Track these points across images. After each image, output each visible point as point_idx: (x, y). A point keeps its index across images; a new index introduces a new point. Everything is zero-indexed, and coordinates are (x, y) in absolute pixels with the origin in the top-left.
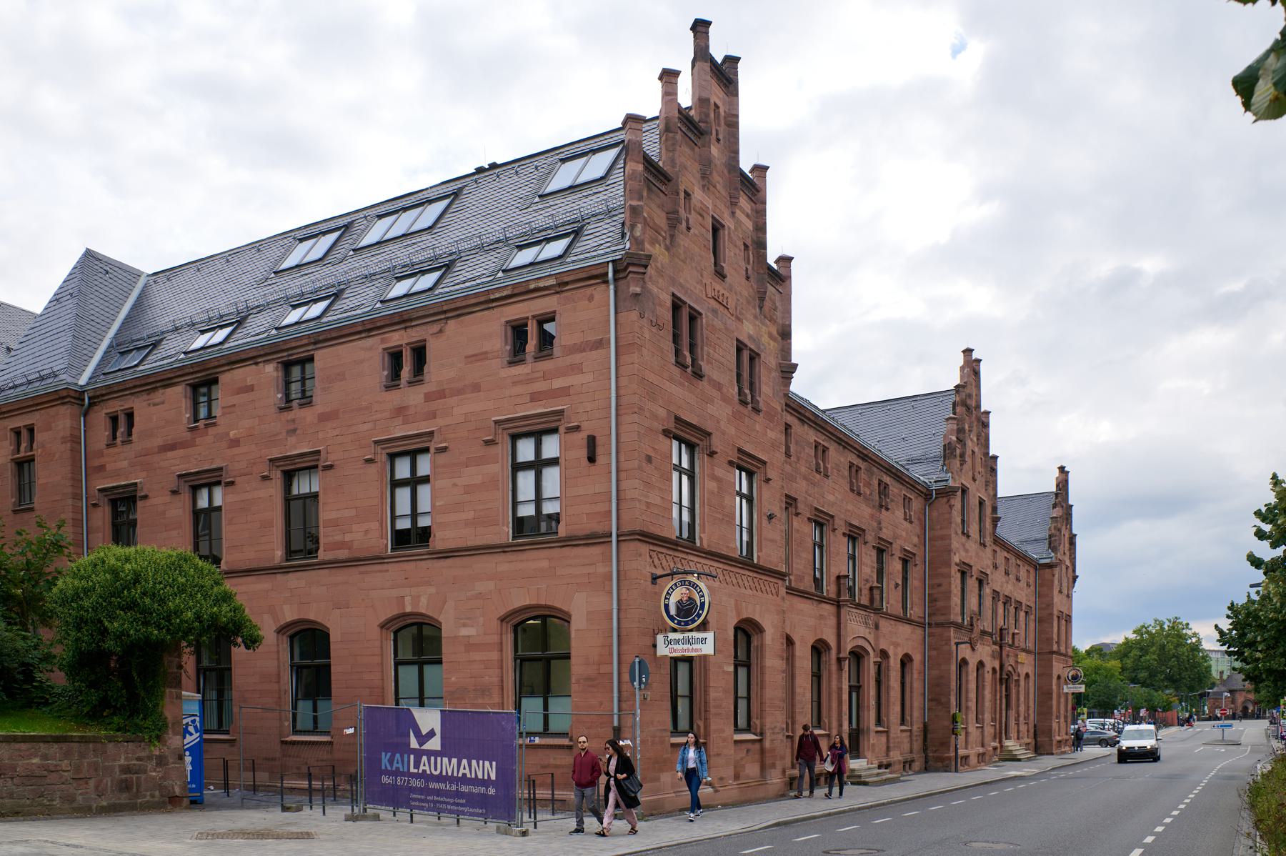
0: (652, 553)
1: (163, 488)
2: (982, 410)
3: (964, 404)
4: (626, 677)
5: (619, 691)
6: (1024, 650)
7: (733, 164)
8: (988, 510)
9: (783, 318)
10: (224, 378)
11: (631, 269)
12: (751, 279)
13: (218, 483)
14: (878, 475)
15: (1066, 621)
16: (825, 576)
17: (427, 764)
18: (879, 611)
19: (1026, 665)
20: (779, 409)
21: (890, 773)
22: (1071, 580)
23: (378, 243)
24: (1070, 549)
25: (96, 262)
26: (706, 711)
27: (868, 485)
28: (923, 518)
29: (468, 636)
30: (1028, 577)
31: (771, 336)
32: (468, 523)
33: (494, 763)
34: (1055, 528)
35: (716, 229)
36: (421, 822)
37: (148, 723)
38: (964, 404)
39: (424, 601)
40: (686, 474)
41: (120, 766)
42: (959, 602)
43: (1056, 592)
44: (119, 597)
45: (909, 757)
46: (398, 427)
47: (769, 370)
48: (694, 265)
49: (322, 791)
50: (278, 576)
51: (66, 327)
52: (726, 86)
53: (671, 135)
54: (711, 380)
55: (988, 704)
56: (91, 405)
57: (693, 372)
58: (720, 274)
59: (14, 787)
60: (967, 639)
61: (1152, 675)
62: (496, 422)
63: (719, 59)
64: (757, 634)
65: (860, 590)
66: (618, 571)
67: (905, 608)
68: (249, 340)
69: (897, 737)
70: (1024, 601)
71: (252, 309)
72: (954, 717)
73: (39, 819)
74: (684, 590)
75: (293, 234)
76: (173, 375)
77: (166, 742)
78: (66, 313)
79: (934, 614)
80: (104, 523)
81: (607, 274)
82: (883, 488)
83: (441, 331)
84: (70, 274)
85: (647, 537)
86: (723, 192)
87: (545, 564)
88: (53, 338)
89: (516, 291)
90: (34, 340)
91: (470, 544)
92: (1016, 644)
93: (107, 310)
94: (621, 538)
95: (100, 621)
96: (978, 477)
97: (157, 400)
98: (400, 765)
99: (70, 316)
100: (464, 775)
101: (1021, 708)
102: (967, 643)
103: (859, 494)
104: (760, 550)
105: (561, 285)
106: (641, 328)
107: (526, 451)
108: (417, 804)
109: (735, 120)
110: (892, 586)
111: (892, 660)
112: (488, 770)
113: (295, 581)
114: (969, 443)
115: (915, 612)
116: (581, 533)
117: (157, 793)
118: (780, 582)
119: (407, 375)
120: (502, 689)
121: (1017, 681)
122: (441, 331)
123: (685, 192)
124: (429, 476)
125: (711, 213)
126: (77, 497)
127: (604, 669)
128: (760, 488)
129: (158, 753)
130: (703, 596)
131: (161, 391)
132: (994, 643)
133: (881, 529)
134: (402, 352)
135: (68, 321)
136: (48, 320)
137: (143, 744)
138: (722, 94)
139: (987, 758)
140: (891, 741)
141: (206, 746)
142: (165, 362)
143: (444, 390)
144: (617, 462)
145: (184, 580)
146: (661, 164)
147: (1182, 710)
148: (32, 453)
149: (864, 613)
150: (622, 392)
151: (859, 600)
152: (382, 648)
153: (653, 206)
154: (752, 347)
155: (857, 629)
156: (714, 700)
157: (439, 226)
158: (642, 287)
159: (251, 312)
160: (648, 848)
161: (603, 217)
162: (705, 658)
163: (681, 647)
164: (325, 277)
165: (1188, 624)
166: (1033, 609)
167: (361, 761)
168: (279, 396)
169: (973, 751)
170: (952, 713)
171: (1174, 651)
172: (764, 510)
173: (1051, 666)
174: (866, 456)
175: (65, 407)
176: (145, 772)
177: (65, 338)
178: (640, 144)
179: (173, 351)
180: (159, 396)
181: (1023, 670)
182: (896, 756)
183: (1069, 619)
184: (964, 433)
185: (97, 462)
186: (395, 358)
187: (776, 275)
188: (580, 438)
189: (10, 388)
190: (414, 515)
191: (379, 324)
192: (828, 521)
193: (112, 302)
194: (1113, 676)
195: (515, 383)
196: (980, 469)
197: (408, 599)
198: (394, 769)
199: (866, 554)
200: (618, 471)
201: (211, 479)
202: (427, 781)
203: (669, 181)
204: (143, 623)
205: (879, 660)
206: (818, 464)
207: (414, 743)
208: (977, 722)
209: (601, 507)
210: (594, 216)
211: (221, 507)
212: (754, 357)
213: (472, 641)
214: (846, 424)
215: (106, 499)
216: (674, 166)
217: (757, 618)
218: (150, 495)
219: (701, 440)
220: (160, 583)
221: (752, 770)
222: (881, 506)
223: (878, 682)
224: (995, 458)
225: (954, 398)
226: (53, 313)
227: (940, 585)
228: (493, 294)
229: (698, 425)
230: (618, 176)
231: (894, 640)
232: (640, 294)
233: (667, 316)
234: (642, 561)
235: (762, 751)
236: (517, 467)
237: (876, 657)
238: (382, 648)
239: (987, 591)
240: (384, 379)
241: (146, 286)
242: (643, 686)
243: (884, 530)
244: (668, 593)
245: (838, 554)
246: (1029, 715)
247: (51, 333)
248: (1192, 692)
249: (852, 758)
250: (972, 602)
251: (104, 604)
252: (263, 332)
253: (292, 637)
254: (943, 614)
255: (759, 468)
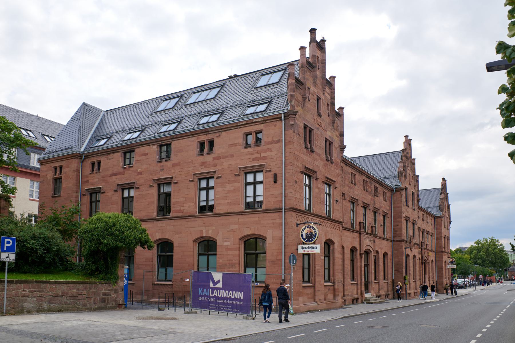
0: (297, 216)
1: (111, 189)
2: (412, 158)
3: (406, 156)
4: (287, 261)
5: (285, 266)
6: (431, 251)
7: (324, 76)
8: (416, 196)
9: (341, 129)
10: (136, 150)
11: (290, 116)
12: (330, 116)
13: (133, 188)
14: (374, 184)
15: (447, 239)
16: (355, 222)
17: (216, 293)
18: (375, 235)
19: (432, 256)
20: (340, 162)
21: (381, 299)
22: (449, 222)
23: (194, 103)
24: (448, 211)
25: (87, 107)
26: (314, 274)
27: (370, 188)
28: (390, 199)
29: (227, 245)
30: (431, 221)
31: (337, 136)
32: (228, 204)
33: (242, 293)
34: (442, 202)
35: (318, 99)
36: (212, 315)
37: (112, 277)
38: (406, 156)
39: (210, 232)
40: (307, 186)
41: (102, 293)
42: (405, 232)
43: (443, 227)
44: (107, 231)
45: (387, 293)
46: (202, 169)
47: (336, 148)
48: (311, 113)
49: (168, 303)
50: (154, 222)
51: (76, 131)
52: (321, 50)
53: (303, 69)
54: (316, 153)
55: (418, 272)
56: (85, 159)
57: (311, 150)
58: (319, 115)
59: (67, 300)
60: (409, 246)
61: (484, 261)
62: (240, 168)
63: (319, 41)
64: (332, 244)
65: (368, 227)
66: (285, 222)
67: (384, 234)
68: (147, 137)
69: (383, 285)
70: (430, 231)
71: (147, 125)
72: (405, 277)
73: (75, 312)
74: (309, 229)
75: (161, 98)
76: (117, 149)
77: (118, 284)
78: (75, 125)
79: (396, 237)
80: (87, 202)
81: (281, 117)
82: (376, 188)
83: (220, 136)
84: (77, 111)
85: (296, 210)
86: (320, 86)
87: (257, 219)
88: (70, 134)
89: (248, 122)
90: (63, 135)
91: (229, 211)
92: (428, 248)
93: (90, 124)
94: (286, 210)
95: (100, 240)
96: (411, 183)
97: (110, 158)
98: (206, 293)
99: (78, 126)
100: (230, 297)
101: (430, 274)
102: (409, 248)
103: (367, 191)
104: (333, 213)
105: (265, 121)
106: (294, 136)
107: (250, 178)
108: (212, 307)
109: (324, 61)
110: (380, 226)
111: (380, 254)
112: (240, 295)
113: (161, 224)
114: (408, 171)
115: (388, 236)
116: (271, 208)
117: (114, 303)
118: (340, 225)
119: (207, 151)
120: (240, 265)
121: (429, 263)
122: (220, 136)
123: (308, 88)
124: (214, 187)
125: (316, 94)
126: (77, 192)
127: (279, 258)
128: (333, 191)
129: (115, 288)
130: (316, 231)
131: (112, 154)
132: (419, 248)
133: (375, 204)
134: (205, 142)
135: (77, 128)
136: (69, 128)
137: (110, 285)
138: (320, 53)
139: (418, 294)
140: (380, 286)
141: (129, 286)
142: (114, 144)
143: (220, 156)
144: (285, 183)
145: (130, 225)
146: (300, 78)
147: (497, 276)
148: (61, 176)
149: (370, 236)
150: (287, 158)
151: (367, 231)
152: (193, 249)
153: (297, 93)
154: (330, 140)
155: (367, 242)
156: (317, 270)
157: (217, 97)
158: (294, 122)
159: (147, 126)
160: (301, 324)
161: (279, 97)
162: (314, 254)
163: (307, 250)
164: (173, 115)
165: (498, 240)
166: (434, 234)
167: (191, 292)
168: (158, 157)
169: (413, 291)
170: (404, 276)
171: (493, 251)
172: (335, 199)
173: (442, 257)
174: (370, 177)
175: (75, 159)
176: (110, 295)
177: (75, 135)
178: (294, 73)
179: (116, 140)
180: (111, 156)
181: (431, 259)
182: (382, 292)
183: (448, 238)
184: (406, 167)
185: (86, 179)
186: (202, 145)
187: (339, 114)
188: (271, 174)
189: (54, 152)
190: (207, 200)
191: (196, 133)
192: (356, 201)
193: (92, 121)
194: (466, 261)
195: (247, 154)
196: (412, 181)
197: (204, 231)
198: (203, 294)
199: (370, 214)
200: (285, 186)
201: (130, 186)
202: (216, 299)
203: (303, 84)
204: (115, 240)
205: (375, 254)
206: (352, 180)
207: (212, 285)
208: (413, 280)
209: (279, 199)
210: (275, 96)
211: (133, 196)
212: (331, 143)
213: (228, 247)
214: (359, 163)
215: (88, 193)
216: (304, 79)
217: (332, 239)
218: (106, 192)
219: (313, 174)
220: (122, 226)
221: (330, 297)
222: (375, 195)
223: (375, 263)
224: (418, 176)
225: (401, 154)
226: (71, 125)
227: (398, 225)
228: (239, 123)
229: (312, 169)
230: (284, 82)
231: (381, 246)
232: (293, 125)
233: (302, 131)
234: (293, 218)
235: (334, 289)
236: (247, 184)
237: (374, 253)
238: (193, 249)
239: (416, 227)
240: (198, 152)
241: (104, 115)
242: (294, 264)
243: (376, 204)
244: (302, 230)
245: (360, 214)
246: (433, 277)
247: (70, 132)
248: (501, 268)
249: (366, 293)
250: (410, 232)
251: (102, 233)
252: (152, 134)
253: (158, 245)
254: (399, 237)
255: (333, 183)
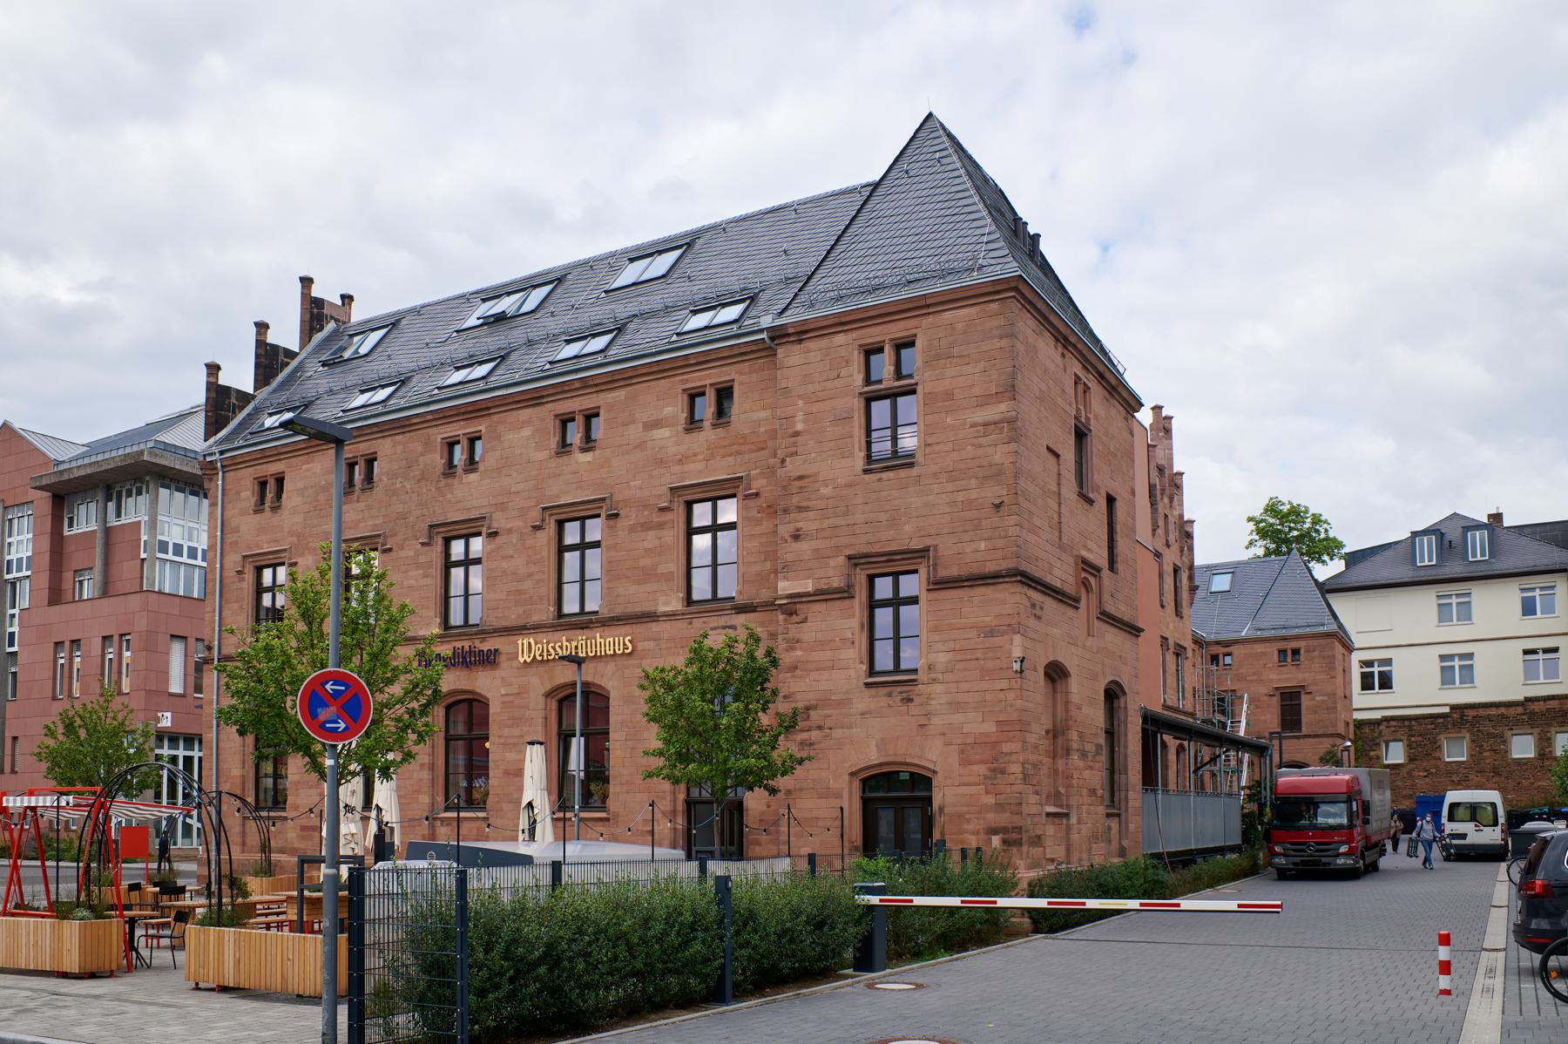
124: (735, 523)
